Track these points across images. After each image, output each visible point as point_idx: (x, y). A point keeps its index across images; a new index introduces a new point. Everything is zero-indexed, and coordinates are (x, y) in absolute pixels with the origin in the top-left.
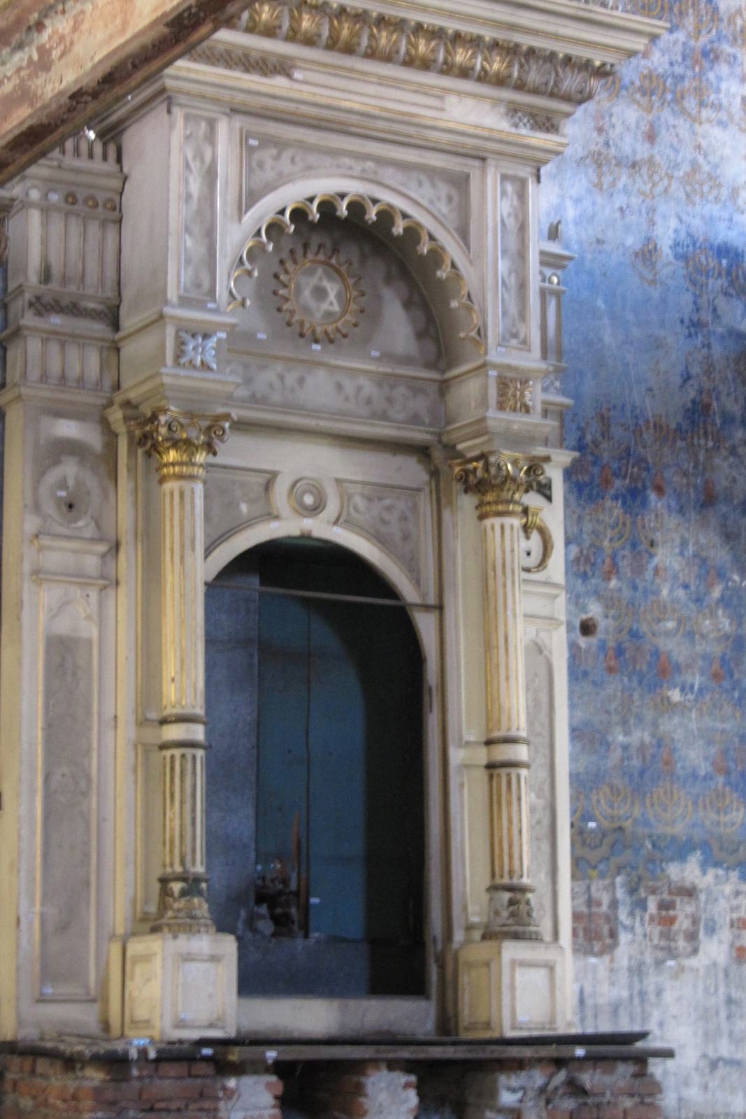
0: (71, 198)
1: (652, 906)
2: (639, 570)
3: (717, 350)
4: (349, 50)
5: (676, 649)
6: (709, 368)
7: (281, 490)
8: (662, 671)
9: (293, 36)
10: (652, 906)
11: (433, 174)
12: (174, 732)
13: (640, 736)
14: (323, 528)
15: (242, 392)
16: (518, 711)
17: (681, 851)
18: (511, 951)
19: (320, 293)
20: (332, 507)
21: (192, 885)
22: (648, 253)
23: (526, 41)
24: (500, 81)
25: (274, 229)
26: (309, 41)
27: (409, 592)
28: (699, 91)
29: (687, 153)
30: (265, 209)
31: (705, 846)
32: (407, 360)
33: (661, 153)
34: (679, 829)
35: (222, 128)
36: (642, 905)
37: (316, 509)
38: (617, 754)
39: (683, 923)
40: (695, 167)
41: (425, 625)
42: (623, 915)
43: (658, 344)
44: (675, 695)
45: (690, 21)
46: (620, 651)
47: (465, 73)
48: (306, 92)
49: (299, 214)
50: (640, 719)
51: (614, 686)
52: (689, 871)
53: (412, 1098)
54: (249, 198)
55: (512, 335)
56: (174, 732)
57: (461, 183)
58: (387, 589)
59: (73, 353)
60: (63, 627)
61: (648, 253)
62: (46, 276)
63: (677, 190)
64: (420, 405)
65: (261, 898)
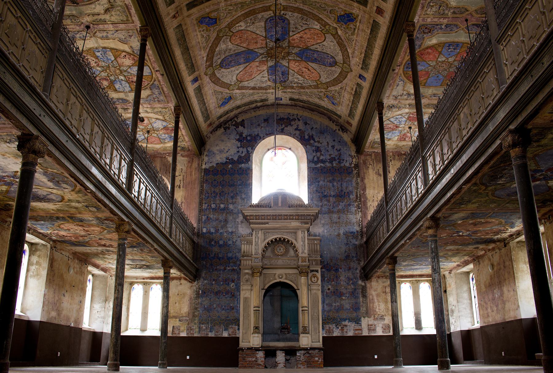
0: (247, 242)
1: (340, 328)
2: (337, 280)
3: (351, 247)
4: (276, 219)
5: (344, 291)
7: (277, 276)
8: (341, 294)
9: (267, 219)
10: (340, 328)
11: (291, 232)
13: (338, 304)
14: (282, 280)
15: (269, 264)
17: (345, 320)
22: (339, 235)
23: (300, 214)
24: (298, 219)
26: (270, 219)
27: (296, 288)
28: (347, 210)
30: (267, 241)
31: (349, 319)
32: (293, 257)
34: (344, 317)
35: (260, 232)
36: (338, 328)
37: (281, 278)
38: (333, 307)
39: (345, 330)
40: (347, 221)
42: (334, 330)
43: (340, 248)
44: (344, 298)
45: (346, 201)
46: (334, 292)
47: (293, 219)
48: (271, 226)
50: (338, 302)
51: (333, 297)
52: (346, 323)
53: (284, 354)
54: (265, 240)
55: (303, 252)
57: (296, 233)
58: (293, 287)
59: (248, 262)
60: (245, 296)
61: (339, 235)
62: (244, 252)
63: (344, 225)
65: (283, 328)
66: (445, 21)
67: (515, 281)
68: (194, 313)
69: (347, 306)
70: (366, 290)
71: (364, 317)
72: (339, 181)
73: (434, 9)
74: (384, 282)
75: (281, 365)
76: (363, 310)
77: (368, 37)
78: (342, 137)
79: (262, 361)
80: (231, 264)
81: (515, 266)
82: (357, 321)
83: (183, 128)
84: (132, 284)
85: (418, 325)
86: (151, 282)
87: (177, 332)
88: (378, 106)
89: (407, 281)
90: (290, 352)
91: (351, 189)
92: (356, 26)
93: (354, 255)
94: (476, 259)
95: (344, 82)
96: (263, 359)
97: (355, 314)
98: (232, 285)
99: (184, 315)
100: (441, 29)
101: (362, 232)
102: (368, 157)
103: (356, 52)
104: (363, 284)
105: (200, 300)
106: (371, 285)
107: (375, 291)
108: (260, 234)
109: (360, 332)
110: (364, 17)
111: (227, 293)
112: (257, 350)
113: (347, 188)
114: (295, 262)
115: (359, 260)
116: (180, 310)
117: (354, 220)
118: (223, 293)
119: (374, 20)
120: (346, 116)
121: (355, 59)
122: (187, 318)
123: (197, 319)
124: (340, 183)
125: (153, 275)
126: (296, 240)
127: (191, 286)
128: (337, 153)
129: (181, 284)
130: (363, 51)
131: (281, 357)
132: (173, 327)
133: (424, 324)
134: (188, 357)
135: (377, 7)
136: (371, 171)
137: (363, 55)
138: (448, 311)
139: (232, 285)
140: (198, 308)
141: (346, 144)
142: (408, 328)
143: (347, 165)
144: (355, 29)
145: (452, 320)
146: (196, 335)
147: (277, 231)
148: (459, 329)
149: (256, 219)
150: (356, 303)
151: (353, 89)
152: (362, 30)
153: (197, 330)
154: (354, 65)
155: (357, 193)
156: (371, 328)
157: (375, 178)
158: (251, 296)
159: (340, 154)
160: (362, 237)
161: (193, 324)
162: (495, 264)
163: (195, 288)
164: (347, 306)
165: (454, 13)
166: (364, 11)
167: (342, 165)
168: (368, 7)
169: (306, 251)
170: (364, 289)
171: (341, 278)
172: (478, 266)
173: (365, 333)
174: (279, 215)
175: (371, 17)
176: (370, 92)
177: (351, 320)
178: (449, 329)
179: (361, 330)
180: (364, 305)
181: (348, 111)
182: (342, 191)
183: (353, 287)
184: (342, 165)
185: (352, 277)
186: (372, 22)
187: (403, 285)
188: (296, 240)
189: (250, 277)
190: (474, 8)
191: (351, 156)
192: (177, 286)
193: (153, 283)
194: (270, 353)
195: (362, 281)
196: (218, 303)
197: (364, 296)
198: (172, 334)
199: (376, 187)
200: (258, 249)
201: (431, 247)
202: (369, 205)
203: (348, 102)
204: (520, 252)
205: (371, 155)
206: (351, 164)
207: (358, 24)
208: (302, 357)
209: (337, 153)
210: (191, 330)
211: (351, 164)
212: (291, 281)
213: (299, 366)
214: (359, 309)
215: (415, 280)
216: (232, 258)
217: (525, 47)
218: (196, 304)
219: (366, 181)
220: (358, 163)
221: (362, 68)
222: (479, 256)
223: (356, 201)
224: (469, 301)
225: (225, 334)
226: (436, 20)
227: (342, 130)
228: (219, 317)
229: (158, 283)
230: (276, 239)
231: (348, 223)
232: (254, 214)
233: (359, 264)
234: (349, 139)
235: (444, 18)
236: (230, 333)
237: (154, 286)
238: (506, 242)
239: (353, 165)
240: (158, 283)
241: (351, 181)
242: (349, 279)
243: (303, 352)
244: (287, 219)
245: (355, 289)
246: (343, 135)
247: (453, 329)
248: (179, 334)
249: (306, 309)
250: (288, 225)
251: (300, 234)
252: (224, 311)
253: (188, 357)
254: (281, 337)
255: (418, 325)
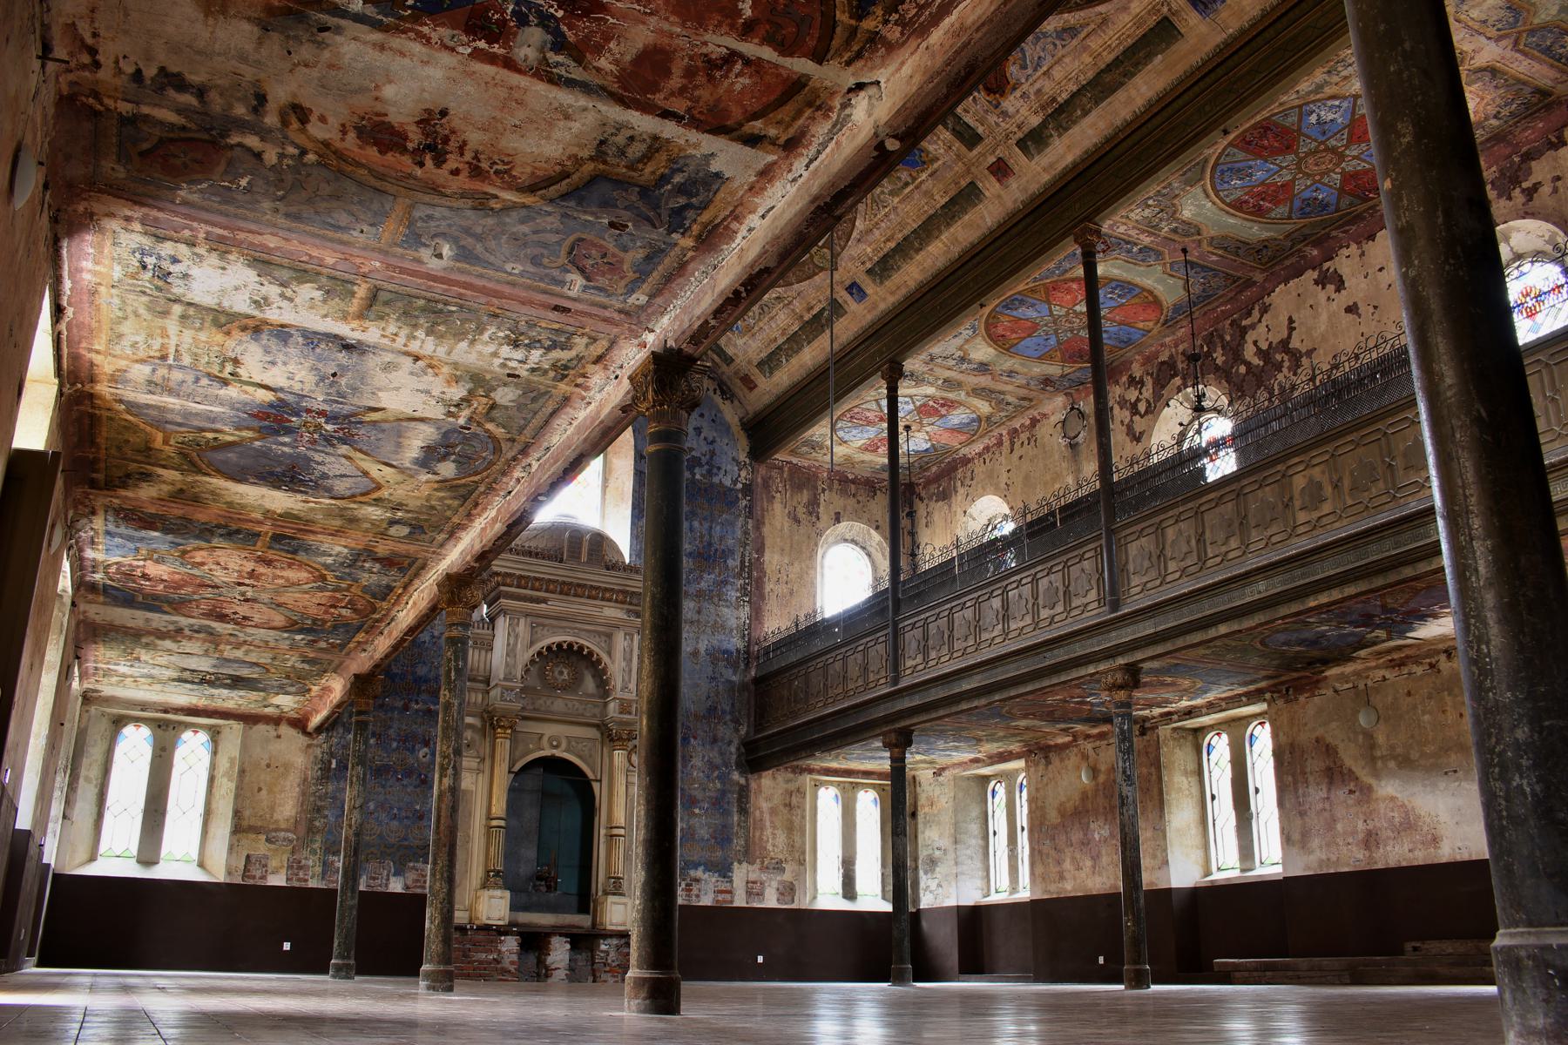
5: (699, 795)
6: (717, 694)
7: (545, 739)
9: (547, 591)
11: (599, 634)
12: (495, 823)
14: (558, 753)
16: (620, 817)
17: (696, 866)
18: (611, 899)
19: (561, 673)
20: (564, 745)
21: (497, 873)
24: (623, 602)
25: (539, 653)
29: (713, 617)
31: (705, 865)
32: (592, 696)
33: (703, 618)
35: (522, 621)
37: (556, 747)
39: (695, 892)
41: (596, 786)
43: (697, 685)
49: (549, 648)
52: (699, 873)
54: (532, 643)
55: (624, 688)
56: (495, 823)
57: (609, 636)
58: (582, 774)
63: (709, 630)
64: (597, 711)
65: (539, 878)
66: (1146, 240)
67: (1162, 809)
68: (311, 821)
69: (704, 833)
70: (747, 797)
71: (740, 862)
72: (705, 519)
73: (1147, 212)
74: (788, 781)
75: (561, 974)
76: (738, 843)
77: (931, 212)
78: (719, 411)
79: (512, 963)
80: (424, 696)
81: (1165, 778)
82: (724, 871)
83: (1443, 517)
84: (119, 722)
85: (849, 890)
86: (180, 723)
87: (258, 874)
88: (891, 368)
89: (831, 783)
90: (584, 941)
91: (730, 542)
92: (914, 179)
93: (728, 709)
94: (1039, 752)
95: (796, 286)
96: (515, 958)
97: (719, 854)
98: (421, 754)
99: (283, 826)
100: (1129, 251)
101: (747, 652)
102: (774, 473)
103: (877, 232)
104: (742, 781)
105: (330, 788)
106: (759, 786)
107: (768, 799)
108: (523, 627)
109: (728, 897)
110: (951, 168)
111: (409, 773)
112: (502, 931)
113: (721, 538)
114: (597, 711)
115: (736, 721)
116: (272, 809)
117: (733, 623)
118: (396, 772)
119: (972, 183)
120: (750, 362)
121: (862, 246)
122: (291, 836)
123: (318, 838)
124: (706, 525)
125: (202, 702)
126: (609, 654)
127: (309, 746)
128: (705, 449)
129: (279, 737)
130: (900, 236)
131: (559, 953)
132: (248, 857)
133: (860, 886)
134: (287, 946)
135: (1000, 159)
136: (777, 506)
137: (892, 245)
138: (916, 860)
139: (421, 754)
140: (323, 807)
141: (727, 429)
142: (827, 896)
143: (728, 482)
144: (907, 184)
145: (924, 880)
146: (313, 884)
147: (564, 624)
148: (954, 903)
149: (518, 587)
150: (724, 826)
151: (810, 309)
152: (926, 193)
153: (318, 869)
154: (852, 258)
155: (743, 555)
156: (754, 890)
157: (786, 525)
158: (485, 792)
159: (713, 453)
160: (747, 665)
161: (305, 853)
162: (1103, 768)
163: (318, 751)
164: (704, 833)
165: (1175, 231)
166: (958, 156)
167: (716, 480)
168: (975, 152)
169: (632, 686)
170: (744, 793)
171: (694, 761)
172: (1041, 767)
173: (740, 901)
174: (579, 585)
175: (968, 171)
176: (871, 331)
177: (710, 867)
178: (916, 900)
179: (730, 892)
180: (741, 833)
181: (763, 355)
182: (710, 544)
183: (719, 786)
184: (716, 480)
185: (718, 761)
186: (963, 183)
187: (822, 792)
188: (609, 654)
189: (477, 737)
190: (1213, 233)
191: (738, 463)
192: (267, 740)
193: (187, 726)
194: (534, 942)
195: (742, 773)
196: (381, 798)
197: (744, 811)
198: (243, 877)
199: (787, 548)
200: (514, 666)
201: (1122, 730)
202: (767, 589)
203: (777, 334)
204: (1177, 750)
205: (781, 468)
206: (735, 482)
207: (924, 176)
208: (612, 954)
209: (705, 449)
210: (300, 868)
211: (735, 482)
212: (580, 757)
213: (604, 976)
214: (729, 840)
215: (851, 781)
216: (427, 681)
217: (1559, 411)
218: (320, 798)
219: (766, 530)
220: (752, 481)
221: (869, 272)
222: (1049, 747)
223: (739, 575)
224: (981, 842)
225: (396, 886)
226: (1133, 233)
227: (723, 393)
228: (381, 836)
229: (202, 727)
230: (559, 645)
231: (719, 627)
232: (518, 573)
233: (737, 730)
234: (736, 419)
235: (1150, 234)
236: (409, 883)
237: (187, 735)
238: (1147, 725)
239: (739, 486)
240: (202, 727)
241: (732, 524)
242: (713, 766)
243: (615, 941)
244: (595, 598)
245: (723, 793)
246: (722, 407)
247: (926, 901)
248: (263, 877)
249: (622, 832)
250: (594, 611)
251: (620, 641)
252: (395, 823)
253: (287, 946)
254: (535, 898)
255: (849, 890)
